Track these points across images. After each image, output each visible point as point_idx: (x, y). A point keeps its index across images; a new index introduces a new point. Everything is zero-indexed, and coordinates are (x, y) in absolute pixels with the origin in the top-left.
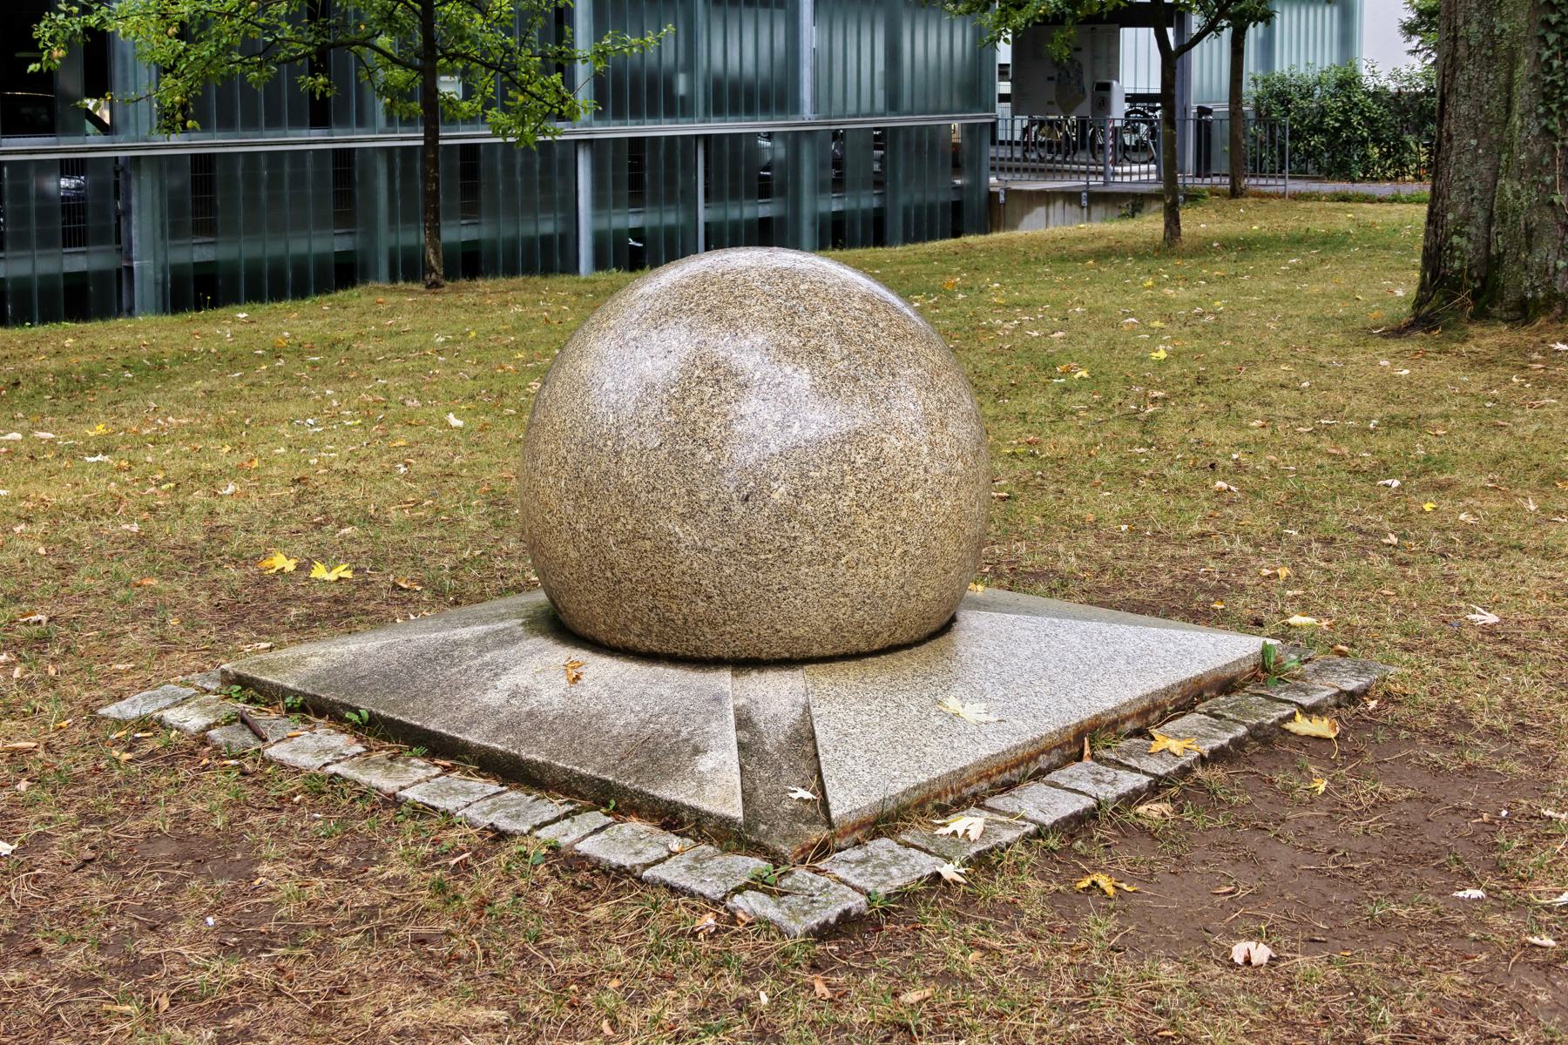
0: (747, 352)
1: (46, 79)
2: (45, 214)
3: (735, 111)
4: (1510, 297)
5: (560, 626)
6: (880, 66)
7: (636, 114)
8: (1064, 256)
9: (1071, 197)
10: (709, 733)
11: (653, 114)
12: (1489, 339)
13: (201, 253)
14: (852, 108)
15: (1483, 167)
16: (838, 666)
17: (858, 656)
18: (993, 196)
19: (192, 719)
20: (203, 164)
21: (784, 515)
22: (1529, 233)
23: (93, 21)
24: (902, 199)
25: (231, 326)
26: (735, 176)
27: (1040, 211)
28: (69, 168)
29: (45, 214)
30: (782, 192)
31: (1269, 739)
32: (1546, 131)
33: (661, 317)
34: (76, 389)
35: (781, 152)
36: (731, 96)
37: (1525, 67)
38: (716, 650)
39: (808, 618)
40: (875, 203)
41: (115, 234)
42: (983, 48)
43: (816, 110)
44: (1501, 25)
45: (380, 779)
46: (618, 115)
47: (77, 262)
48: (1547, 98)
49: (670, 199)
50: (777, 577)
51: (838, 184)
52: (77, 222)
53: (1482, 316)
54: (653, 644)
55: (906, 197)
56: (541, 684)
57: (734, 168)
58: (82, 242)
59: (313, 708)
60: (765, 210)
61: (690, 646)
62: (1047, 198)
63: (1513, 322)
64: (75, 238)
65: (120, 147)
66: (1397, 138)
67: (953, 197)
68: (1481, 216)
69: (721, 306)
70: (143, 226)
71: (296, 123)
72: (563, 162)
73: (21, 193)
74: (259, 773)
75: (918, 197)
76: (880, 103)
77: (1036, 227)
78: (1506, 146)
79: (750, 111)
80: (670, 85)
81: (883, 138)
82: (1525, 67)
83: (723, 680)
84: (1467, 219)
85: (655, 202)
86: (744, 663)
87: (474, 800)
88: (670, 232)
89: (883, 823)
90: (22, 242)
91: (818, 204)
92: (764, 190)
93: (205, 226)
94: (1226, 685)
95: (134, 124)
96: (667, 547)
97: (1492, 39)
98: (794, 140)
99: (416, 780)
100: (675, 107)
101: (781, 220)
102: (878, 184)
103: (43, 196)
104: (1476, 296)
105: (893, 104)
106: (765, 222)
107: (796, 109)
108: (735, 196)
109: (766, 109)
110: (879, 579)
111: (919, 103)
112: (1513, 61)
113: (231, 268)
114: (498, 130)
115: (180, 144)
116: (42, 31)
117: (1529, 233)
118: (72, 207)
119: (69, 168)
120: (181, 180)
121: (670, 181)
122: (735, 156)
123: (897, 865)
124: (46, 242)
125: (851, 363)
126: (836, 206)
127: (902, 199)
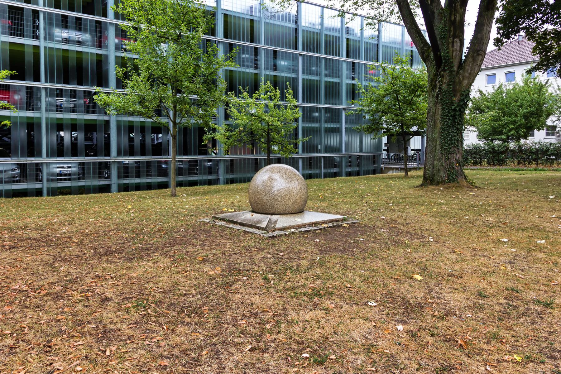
0: (276, 176)
1: (205, 146)
2: (205, 169)
3: (329, 152)
4: (436, 181)
5: (253, 211)
6: (358, 144)
7: (310, 152)
8: (391, 178)
9: (397, 169)
10: (264, 220)
11: (314, 152)
12: (431, 188)
13: (231, 176)
14: (355, 151)
15: (432, 159)
16: (289, 216)
17: (287, 214)
18: (382, 168)
19: (208, 221)
20: (232, 160)
21: (277, 195)
22: (439, 170)
23: (212, 136)
24: (363, 169)
25: (231, 186)
26: (329, 164)
27: (391, 171)
28: (209, 161)
29: (205, 169)
30: (339, 167)
31: (339, 226)
32: (442, 153)
33: (266, 171)
34: (205, 193)
35: (339, 159)
36: (328, 149)
37: (438, 143)
38: (269, 212)
39: (280, 208)
40: (358, 169)
41: (217, 173)
42: (380, 141)
43: (346, 151)
44: (434, 135)
45: (228, 226)
46: (307, 152)
47: (210, 177)
48: (442, 148)
49: (317, 168)
50: (276, 203)
51: (350, 166)
52: (210, 171)
53: (431, 184)
54: (262, 212)
55: (364, 169)
56: (248, 216)
57: (330, 162)
58: (211, 174)
59: (222, 219)
60: (335, 170)
61: (266, 212)
62: (392, 169)
63: (436, 185)
64: (210, 173)
65: (218, 158)
66: (466, 157)
67: (374, 169)
68: (432, 168)
69: (272, 171)
70: (221, 171)
71: (248, 154)
72: (297, 162)
73: (201, 165)
74: (214, 226)
75: (366, 169)
76: (358, 151)
77: (390, 173)
78: (435, 156)
79: (332, 152)
80: (317, 147)
81: (359, 157)
82: (438, 143)
83: (269, 216)
84: (429, 168)
85: (314, 168)
86: (272, 214)
87: (237, 227)
88: (317, 174)
89: (282, 229)
90: (201, 174)
91: (346, 169)
92: (335, 166)
93: (232, 172)
94: (337, 221)
95: (219, 154)
96: (263, 199)
97: (433, 138)
98: (341, 157)
99: (232, 226)
100: (318, 151)
101: (339, 172)
102: (358, 166)
103: (204, 166)
104: (431, 181)
105: (361, 150)
106: (335, 173)
107: (342, 151)
108: (329, 167)
109: (336, 152)
110: (289, 204)
111: (366, 151)
112: (436, 141)
113: (237, 178)
114: (283, 155)
115: (227, 157)
116: (204, 138)
117: (439, 170)
118: (209, 168)
119: (209, 161)
120: (228, 164)
121: (317, 165)
122: (329, 160)
123: (282, 232)
124: (205, 174)
125: (289, 178)
126: (350, 170)
127: (363, 169)
